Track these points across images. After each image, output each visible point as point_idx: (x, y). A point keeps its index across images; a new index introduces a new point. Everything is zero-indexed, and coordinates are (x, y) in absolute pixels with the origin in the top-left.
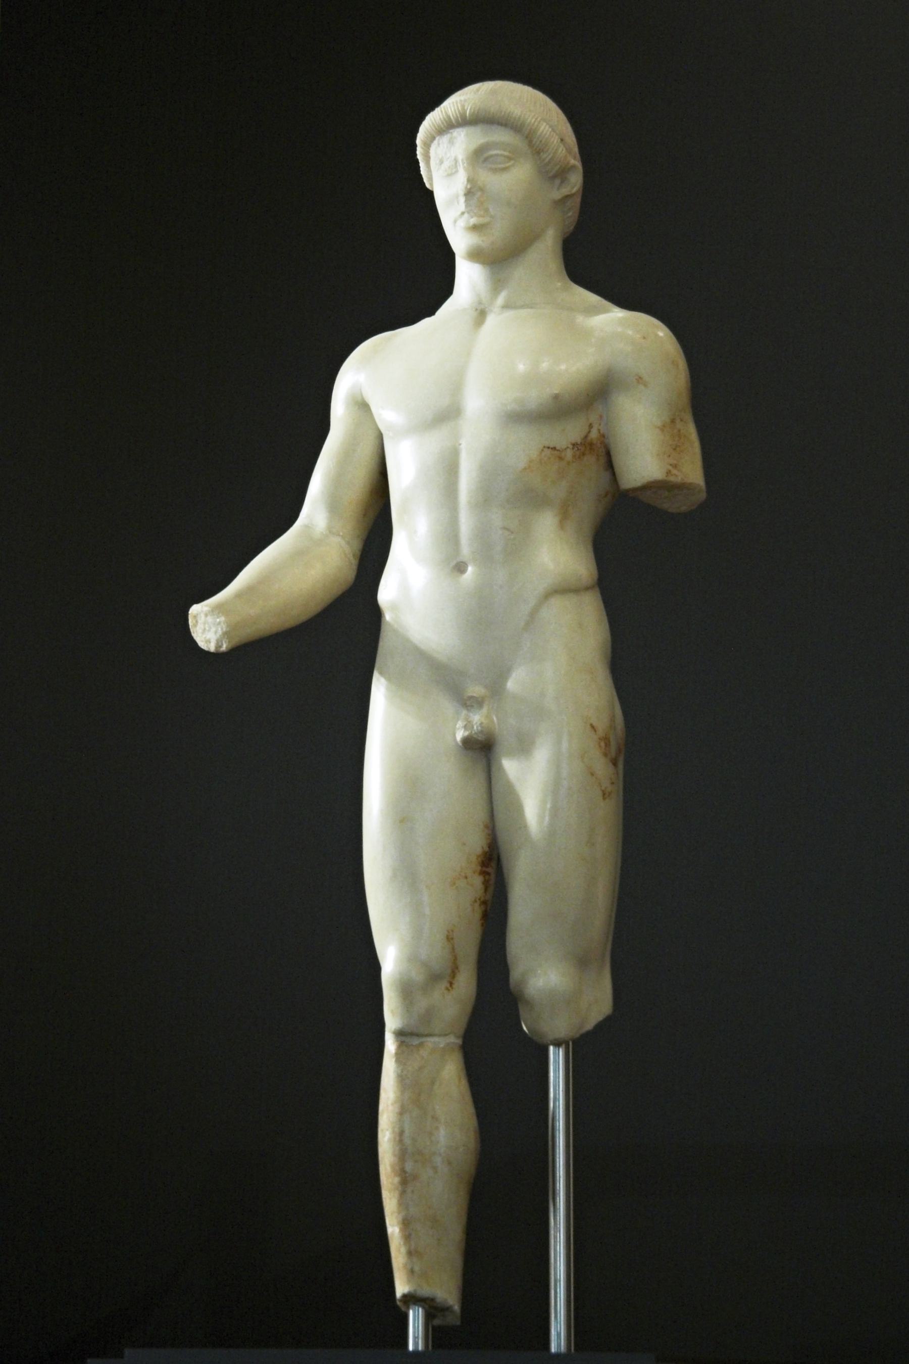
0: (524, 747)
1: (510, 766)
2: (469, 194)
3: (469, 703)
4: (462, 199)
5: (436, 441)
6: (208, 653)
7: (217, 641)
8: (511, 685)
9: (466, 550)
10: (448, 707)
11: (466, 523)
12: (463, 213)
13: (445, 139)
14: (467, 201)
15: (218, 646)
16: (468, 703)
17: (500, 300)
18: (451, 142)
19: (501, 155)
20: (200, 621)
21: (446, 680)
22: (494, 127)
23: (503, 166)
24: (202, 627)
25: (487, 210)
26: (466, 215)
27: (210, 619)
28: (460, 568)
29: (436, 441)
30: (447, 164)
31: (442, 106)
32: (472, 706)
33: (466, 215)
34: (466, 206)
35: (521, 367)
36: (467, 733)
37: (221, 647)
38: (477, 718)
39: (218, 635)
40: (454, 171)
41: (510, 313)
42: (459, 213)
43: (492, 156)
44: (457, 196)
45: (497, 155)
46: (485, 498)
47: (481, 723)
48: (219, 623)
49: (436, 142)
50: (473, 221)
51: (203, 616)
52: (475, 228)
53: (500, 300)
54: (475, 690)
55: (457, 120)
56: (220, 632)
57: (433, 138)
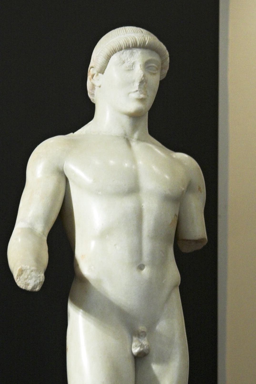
0: (164, 360)
1: (156, 368)
2: (141, 82)
3: (134, 333)
4: (137, 84)
5: (128, 204)
6: (25, 292)
7: (35, 285)
8: (158, 328)
9: (146, 258)
10: (127, 335)
11: (147, 246)
12: (137, 91)
13: (128, 52)
14: (140, 85)
15: (34, 287)
16: (141, 334)
17: (136, 136)
18: (132, 54)
19: (155, 67)
20: (23, 275)
21: (128, 322)
22: (154, 53)
23: (154, 72)
24: (26, 277)
25: (146, 92)
26: (138, 92)
27: (33, 274)
28: (141, 267)
29: (128, 204)
30: (126, 65)
31: (176, 299)
32: (142, 336)
33: (138, 92)
34: (139, 88)
35: (126, 165)
36: (142, 349)
37: (34, 288)
38: (145, 342)
39: (36, 282)
40: (131, 69)
41: (142, 144)
42: (135, 90)
43: (151, 66)
44: (134, 82)
45: (154, 66)
46: (156, 235)
47: (148, 345)
48: (40, 277)
50: (142, 96)
51: (28, 272)
52: (142, 100)
53: (136, 136)
54: (141, 328)
55: (140, 45)
56: (38, 281)
57: (121, 49)
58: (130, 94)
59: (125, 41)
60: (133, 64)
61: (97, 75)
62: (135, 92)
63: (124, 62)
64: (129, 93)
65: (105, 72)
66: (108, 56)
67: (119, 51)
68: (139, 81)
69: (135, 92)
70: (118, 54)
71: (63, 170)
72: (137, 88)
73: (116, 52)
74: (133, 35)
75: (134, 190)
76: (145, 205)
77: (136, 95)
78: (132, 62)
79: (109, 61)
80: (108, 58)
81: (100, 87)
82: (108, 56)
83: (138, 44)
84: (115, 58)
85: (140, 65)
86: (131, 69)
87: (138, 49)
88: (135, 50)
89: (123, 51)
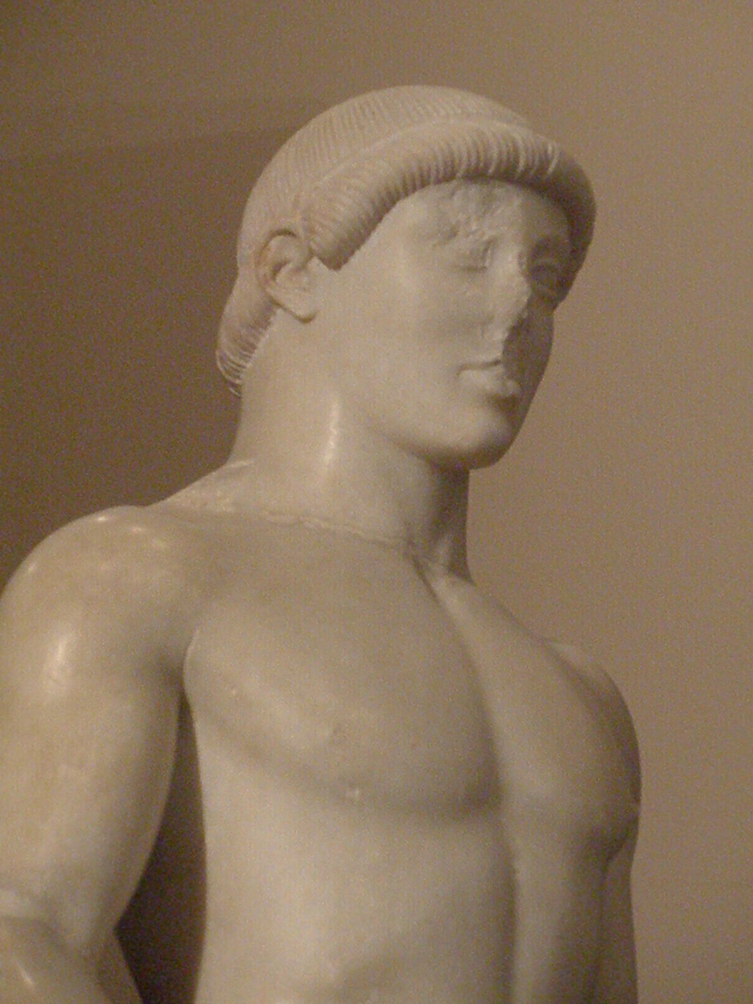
4: (499, 335)
5: (448, 862)
12: (496, 363)
13: (474, 191)
14: (509, 341)
18: (487, 203)
26: (500, 369)
29: (448, 862)
30: (463, 244)
33: (500, 369)
34: (506, 351)
44: (486, 322)
49: (447, 187)
57: (448, 176)
58: (466, 374)
59: (475, 144)
60: (491, 245)
61: (302, 268)
62: (486, 366)
63: (453, 234)
64: (463, 368)
65: (354, 260)
66: (389, 193)
67: (438, 182)
68: (510, 323)
69: (486, 366)
70: (432, 193)
71: (181, 669)
72: (497, 353)
73: (424, 184)
74: (501, 126)
75: (479, 795)
76: (525, 872)
77: (486, 381)
78: (486, 238)
79: (380, 219)
80: (385, 203)
81: (306, 320)
82: (389, 193)
83: (551, 169)
84: (412, 211)
85: (520, 256)
86: (475, 266)
87: (510, 187)
88: (500, 190)
89: (455, 183)
